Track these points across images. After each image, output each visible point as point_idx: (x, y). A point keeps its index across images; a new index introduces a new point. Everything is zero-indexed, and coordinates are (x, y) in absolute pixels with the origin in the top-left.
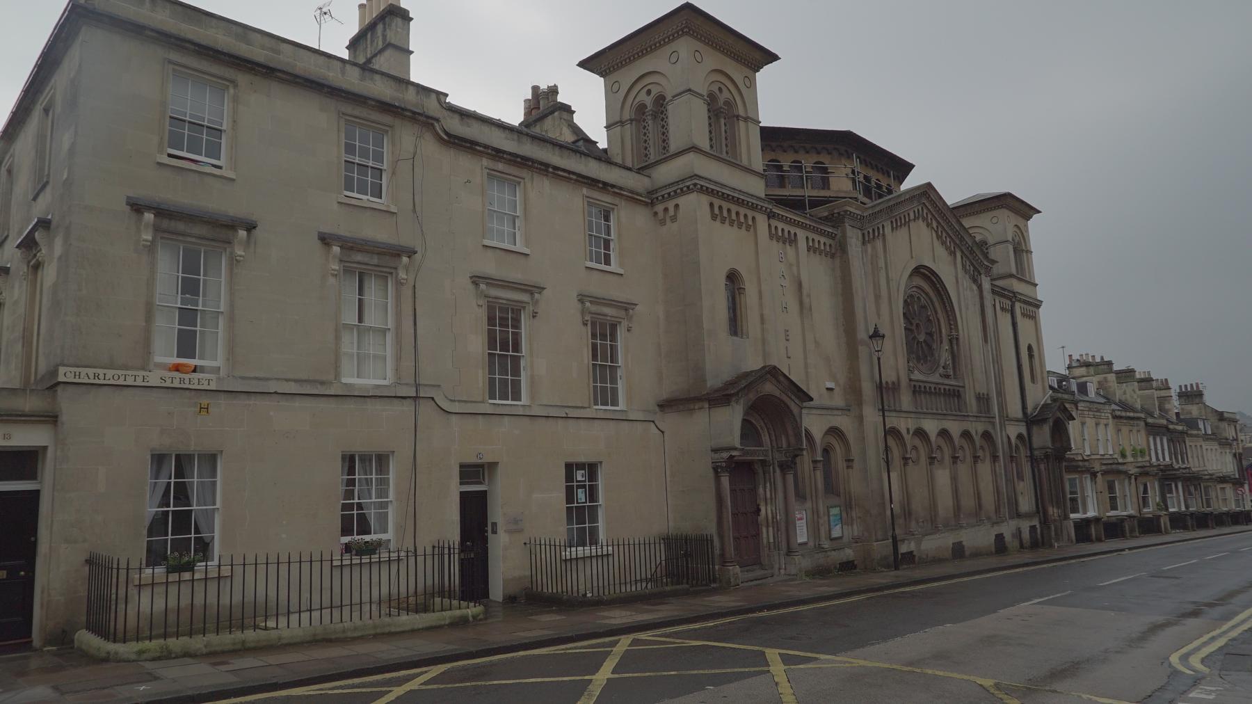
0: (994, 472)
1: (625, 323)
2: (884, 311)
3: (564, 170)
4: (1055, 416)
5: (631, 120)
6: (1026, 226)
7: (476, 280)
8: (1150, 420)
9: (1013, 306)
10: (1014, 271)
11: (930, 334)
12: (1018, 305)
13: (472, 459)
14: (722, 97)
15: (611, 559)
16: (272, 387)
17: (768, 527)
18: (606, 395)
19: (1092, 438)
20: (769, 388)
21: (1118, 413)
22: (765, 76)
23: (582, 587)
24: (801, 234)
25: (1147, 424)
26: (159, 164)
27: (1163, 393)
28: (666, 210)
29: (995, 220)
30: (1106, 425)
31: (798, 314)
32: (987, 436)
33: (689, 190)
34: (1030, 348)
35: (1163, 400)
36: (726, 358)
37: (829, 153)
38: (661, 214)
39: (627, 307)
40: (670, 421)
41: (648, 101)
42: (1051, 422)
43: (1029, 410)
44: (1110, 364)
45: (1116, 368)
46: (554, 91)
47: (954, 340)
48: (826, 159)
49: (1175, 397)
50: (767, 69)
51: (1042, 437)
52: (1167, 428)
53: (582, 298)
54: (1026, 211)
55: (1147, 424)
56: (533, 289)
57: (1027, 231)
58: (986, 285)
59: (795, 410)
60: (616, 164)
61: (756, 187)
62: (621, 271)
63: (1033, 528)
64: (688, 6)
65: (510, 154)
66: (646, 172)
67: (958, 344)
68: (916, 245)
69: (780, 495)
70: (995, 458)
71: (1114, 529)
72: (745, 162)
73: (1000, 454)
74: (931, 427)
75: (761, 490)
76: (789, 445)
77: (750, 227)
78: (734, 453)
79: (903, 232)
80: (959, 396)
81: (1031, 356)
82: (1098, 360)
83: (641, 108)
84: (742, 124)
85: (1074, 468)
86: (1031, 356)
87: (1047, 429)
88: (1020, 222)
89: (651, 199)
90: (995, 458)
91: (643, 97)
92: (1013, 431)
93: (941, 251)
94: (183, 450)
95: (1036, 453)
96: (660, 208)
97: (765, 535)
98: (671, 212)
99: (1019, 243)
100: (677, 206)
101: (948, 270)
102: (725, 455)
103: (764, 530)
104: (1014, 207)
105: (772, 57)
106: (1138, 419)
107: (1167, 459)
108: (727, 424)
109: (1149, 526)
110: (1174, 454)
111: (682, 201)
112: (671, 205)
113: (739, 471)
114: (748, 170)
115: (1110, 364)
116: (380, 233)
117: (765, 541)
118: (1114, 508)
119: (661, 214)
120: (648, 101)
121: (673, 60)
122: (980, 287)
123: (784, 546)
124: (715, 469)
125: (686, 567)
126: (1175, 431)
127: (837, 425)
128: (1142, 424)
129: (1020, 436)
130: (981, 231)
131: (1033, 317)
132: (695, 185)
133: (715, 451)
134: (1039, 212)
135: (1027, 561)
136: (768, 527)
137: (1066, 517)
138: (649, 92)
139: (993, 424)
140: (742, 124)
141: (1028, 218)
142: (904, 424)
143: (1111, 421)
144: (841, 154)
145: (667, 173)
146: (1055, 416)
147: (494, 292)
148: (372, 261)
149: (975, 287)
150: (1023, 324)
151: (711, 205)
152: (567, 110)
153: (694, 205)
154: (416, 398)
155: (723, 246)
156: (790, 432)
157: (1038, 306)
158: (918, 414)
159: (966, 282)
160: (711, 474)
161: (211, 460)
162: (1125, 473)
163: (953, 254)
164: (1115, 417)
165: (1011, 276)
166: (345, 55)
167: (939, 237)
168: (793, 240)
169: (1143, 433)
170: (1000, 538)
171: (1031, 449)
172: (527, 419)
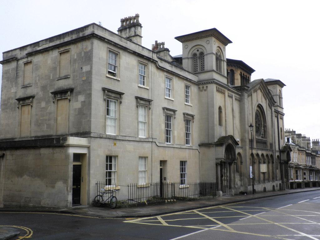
0: (272, 166)
1: (192, 121)
2: (251, 118)
3: (183, 76)
4: (287, 150)
5: (191, 58)
6: (224, 48)
7: (164, 109)
8: (307, 151)
9: (278, 115)
10: (279, 105)
11: (259, 125)
12: (279, 115)
13: (162, 159)
14: (219, 54)
15: (188, 189)
16: (127, 138)
17: (225, 181)
18: (187, 142)
19: (296, 158)
20: (230, 142)
21: (299, 149)
22: (229, 47)
23: (186, 195)
24: (234, 95)
25: (306, 152)
26: (107, 77)
27: (308, 142)
28: (203, 87)
29: (274, 88)
30: (296, 152)
31: (233, 120)
32: (272, 156)
33: (212, 83)
34: (220, 108)
35: (309, 144)
36: (219, 132)
37: (235, 67)
38: (201, 89)
39: (193, 116)
40: (204, 149)
41: (198, 53)
42: (286, 152)
43: (281, 148)
44: (295, 132)
45: (296, 133)
46: (163, 44)
47: (265, 126)
48: (234, 69)
49: (311, 143)
50: (229, 45)
51: (284, 157)
52: (311, 154)
53: (184, 114)
54: (281, 85)
55: (306, 152)
56: (174, 111)
57: (225, 51)
58: (273, 110)
59: (234, 147)
60: (185, 70)
61: (224, 81)
62: (192, 105)
63: (280, 184)
64: (215, 30)
65: (190, 79)
66: (197, 75)
67: (266, 128)
68: (258, 98)
69: (228, 172)
70: (273, 162)
71: (299, 185)
72: (223, 74)
73: (274, 161)
74: (260, 153)
75: (223, 170)
76: (232, 158)
77: (224, 93)
78: (222, 160)
79: (255, 93)
80: (266, 144)
81: (281, 131)
82: (291, 130)
83: (195, 55)
84: (222, 62)
85: (290, 167)
86: (281, 131)
87: (286, 154)
88: (222, 46)
89: (198, 84)
90: (273, 162)
91: (196, 51)
92: (277, 154)
93: (264, 99)
94: (111, 155)
95: (282, 161)
96: (201, 86)
97: (224, 183)
98: (205, 88)
99: (220, 56)
100: (207, 87)
101: (265, 105)
102: (220, 160)
103: (224, 182)
104: (280, 84)
105: (230, 42)
106: (304, 151)
107: (311, 164)
108: (221, 152)
109: (307, 185)
110: (312, 162)
111: (209, 86)
112: (205, 86)
113: (221, 164)
114: (224, 76)
115: (295, 132)
116: (145, 96)
117: (224, 185)
118: (297, 179)
119: (201, 89)
120: (198, 53)
121: (208, 43)
122: (271, 110)
123: (228, 186)
124: (217, 164)
125: (206, 190)
126: (313, 155)
127: (240, 152)
128: (305, 152)
129: (278, 156)
130: (203, 48)
131: (282, 119)
132: (214, 82)
133: (216, 159)
134: (286, 85)
135: (269, 195)
136: (225, 181)
137: (288, 181)
138: (198, 50)
139: (273, 152)
140: (222, 62)
141: (226, 45)
142: (254, 152)
143: (297, 151)
144: (238, 67)
145: (204, 77)
146: (287, 150)
147: (168, 112)
148: (144, 102)
149: (270, 110)
150: (280, 121)
151: (217, 87)
152: (167, 50)
153: (213, 88)
154: (152, 142)
155: (219, 99)
156: (233, 154)
157: (283, 115)
158: (258, 149)
159: (268, 108)
160: (215, 166)
161: (116, 157)
162: (301, 168)
163: (266, 100)
164: (298, 150)
165: (278, 106)
166: (117, 33)
167: (263, 95)
168: (224, 93)
169: (305, 155)
170: (265, 188)
171: (280, 160)
172: (173, 148)
